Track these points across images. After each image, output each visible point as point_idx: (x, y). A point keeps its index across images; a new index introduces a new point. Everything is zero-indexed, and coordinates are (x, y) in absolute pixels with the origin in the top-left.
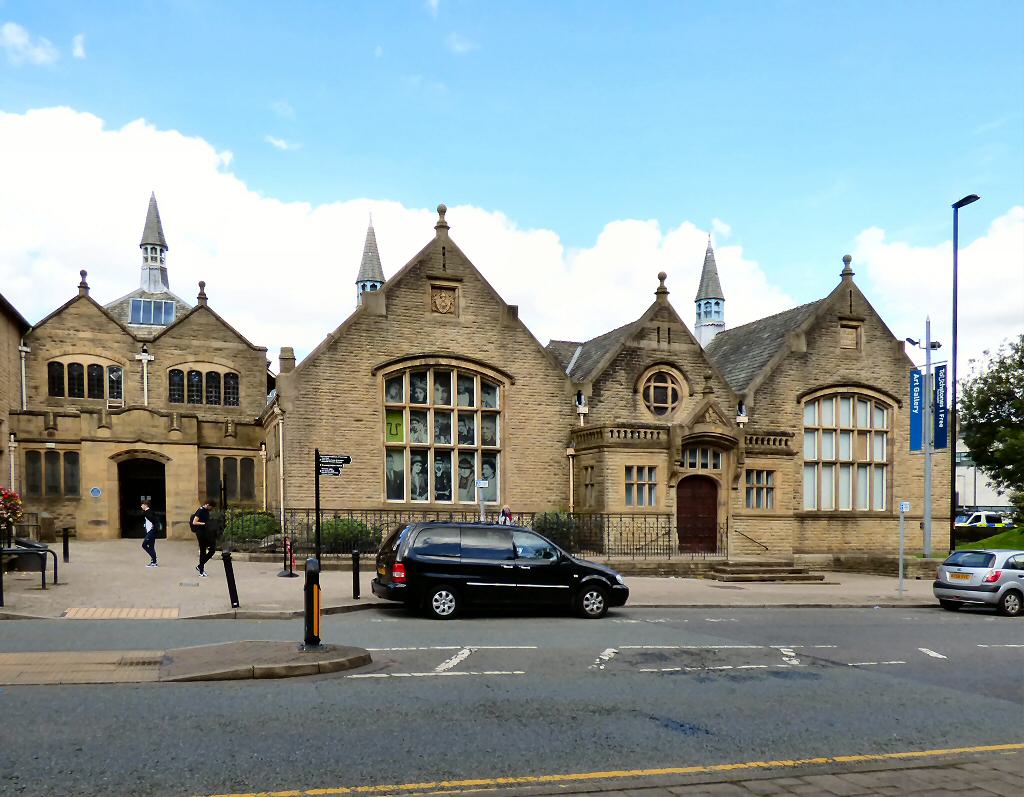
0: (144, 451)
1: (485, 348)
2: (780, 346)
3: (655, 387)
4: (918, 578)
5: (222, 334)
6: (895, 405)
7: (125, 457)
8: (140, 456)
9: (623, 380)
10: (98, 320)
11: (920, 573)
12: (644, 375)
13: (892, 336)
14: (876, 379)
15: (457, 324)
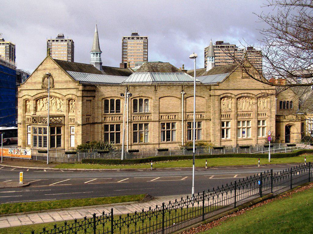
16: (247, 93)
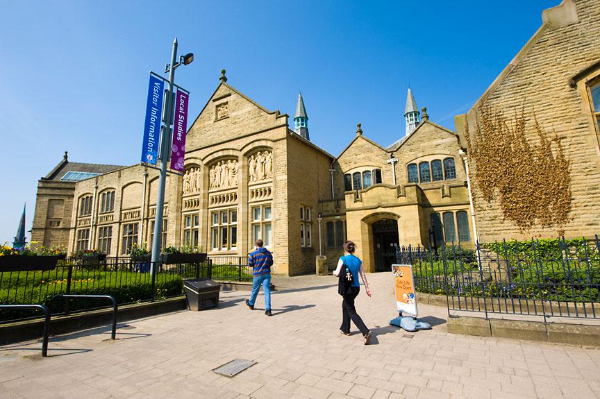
0: (383, 213)
2: (229, 170)
5: (439, 135)
7: (372, 220)
8: (381, 217)
10: (366, 146)
13: (355, 311)
16: (223, 150)
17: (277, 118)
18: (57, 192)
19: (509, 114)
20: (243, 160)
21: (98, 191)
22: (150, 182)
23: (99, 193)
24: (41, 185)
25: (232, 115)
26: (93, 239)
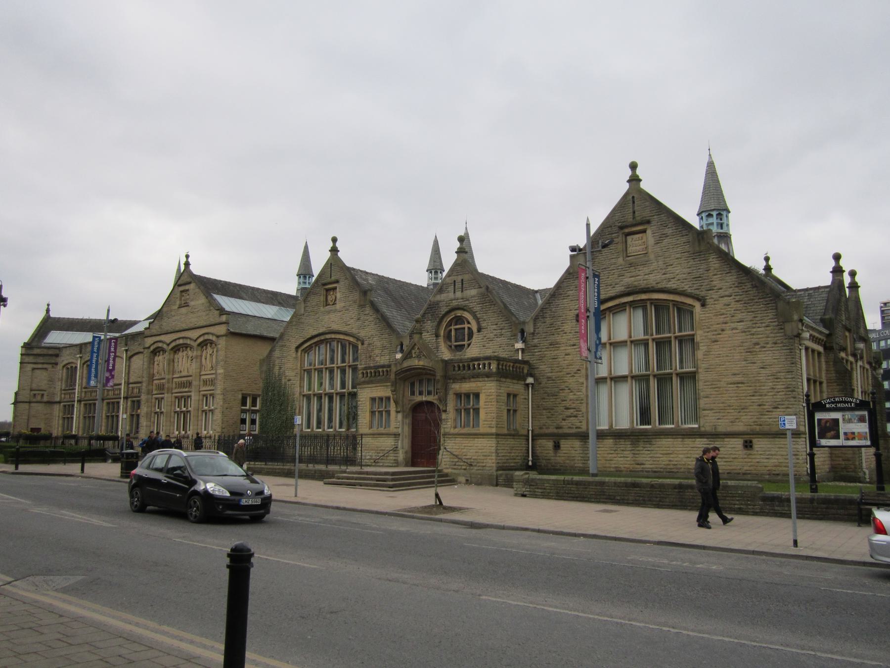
1: (349, 323)
3: (456, 329)
4: (524, 496)
6: (697, 305)
9: (429, 328)
11: (524, 490)
12: (445, 320)
14: (669, 280)
15: (335, 311)
16: (183, 338)
17: (220, 315)
18: (40, 360)
19: (277, 362)
20: (169, 354)
21: (83, 362)
22: (131, 357)
23: (84, 364)
24: (23, 352)
25: (192, 303)
26: (114, 423)
